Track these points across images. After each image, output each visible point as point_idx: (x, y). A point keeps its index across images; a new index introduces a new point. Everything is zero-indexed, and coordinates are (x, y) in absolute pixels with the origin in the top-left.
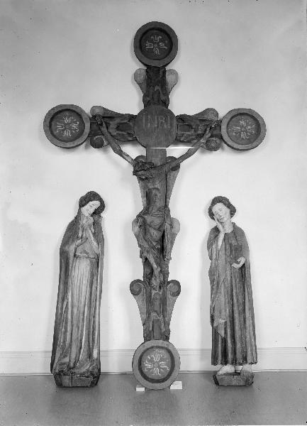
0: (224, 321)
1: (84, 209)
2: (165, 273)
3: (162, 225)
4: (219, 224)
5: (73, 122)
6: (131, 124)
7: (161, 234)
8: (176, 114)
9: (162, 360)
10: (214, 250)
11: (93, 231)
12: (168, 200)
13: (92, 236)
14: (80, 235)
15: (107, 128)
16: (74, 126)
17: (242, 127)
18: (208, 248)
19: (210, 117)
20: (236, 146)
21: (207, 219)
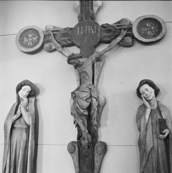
1: (20, 93)
5: (34, 36)
8: (100, 24)
16: (34, 39)
17: (148, 27)
18: (137, 122)
20: (158, 38)
21: (137, 98)
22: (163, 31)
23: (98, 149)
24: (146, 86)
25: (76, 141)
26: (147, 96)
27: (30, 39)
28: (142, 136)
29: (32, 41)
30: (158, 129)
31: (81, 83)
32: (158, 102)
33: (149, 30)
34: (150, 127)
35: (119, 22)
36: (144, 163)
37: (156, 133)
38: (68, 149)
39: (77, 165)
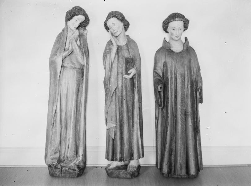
0: (114, 125)
11: (79, 44)
13: (77, 48)
18: (104, 60)
24: (113, 20)
26: (115, 32)
28: (107, 76)
30: (124, 68)
34: (115, 65)
37: (122, 73)
38: (194, 50)
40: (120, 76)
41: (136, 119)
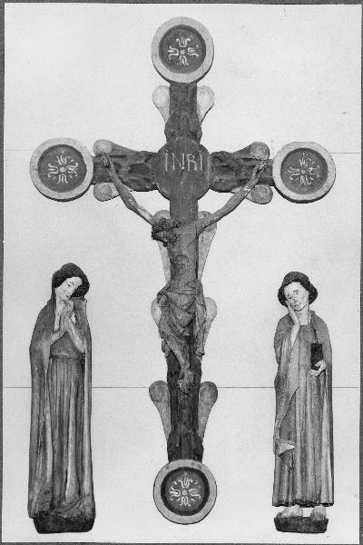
1: (58, 290)
2: (197, 369)
3: (192, 305)
4: (292, 312)
5: (69, 163)
6: (149, 165)
7: (189, 317)
8: (211, 150)
9: (192, 485)
10: (284, 349)
11: (75, 321)
12: (199, 272)
14: (56, 327)
15: (117, 171)
16: (72, 169)
17: (303, 168)
19: (258, 154)
22: (330, 180)
23: (205, 397)
24: (295, 286)
25: (165, 379)
27: (62, 170)
29: (67, 173)
31: (173, 277)
32: (313, 313)
33: (304, 175)
35: (248, 150)
36: (282, 413)
39: (168, 421)
40: (303, 371)
41: (325, 439)
